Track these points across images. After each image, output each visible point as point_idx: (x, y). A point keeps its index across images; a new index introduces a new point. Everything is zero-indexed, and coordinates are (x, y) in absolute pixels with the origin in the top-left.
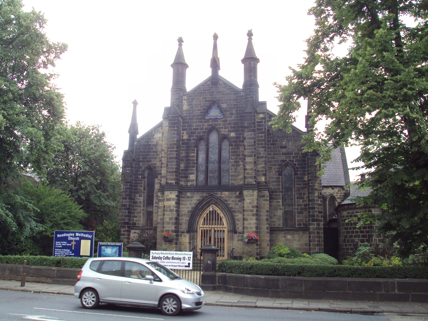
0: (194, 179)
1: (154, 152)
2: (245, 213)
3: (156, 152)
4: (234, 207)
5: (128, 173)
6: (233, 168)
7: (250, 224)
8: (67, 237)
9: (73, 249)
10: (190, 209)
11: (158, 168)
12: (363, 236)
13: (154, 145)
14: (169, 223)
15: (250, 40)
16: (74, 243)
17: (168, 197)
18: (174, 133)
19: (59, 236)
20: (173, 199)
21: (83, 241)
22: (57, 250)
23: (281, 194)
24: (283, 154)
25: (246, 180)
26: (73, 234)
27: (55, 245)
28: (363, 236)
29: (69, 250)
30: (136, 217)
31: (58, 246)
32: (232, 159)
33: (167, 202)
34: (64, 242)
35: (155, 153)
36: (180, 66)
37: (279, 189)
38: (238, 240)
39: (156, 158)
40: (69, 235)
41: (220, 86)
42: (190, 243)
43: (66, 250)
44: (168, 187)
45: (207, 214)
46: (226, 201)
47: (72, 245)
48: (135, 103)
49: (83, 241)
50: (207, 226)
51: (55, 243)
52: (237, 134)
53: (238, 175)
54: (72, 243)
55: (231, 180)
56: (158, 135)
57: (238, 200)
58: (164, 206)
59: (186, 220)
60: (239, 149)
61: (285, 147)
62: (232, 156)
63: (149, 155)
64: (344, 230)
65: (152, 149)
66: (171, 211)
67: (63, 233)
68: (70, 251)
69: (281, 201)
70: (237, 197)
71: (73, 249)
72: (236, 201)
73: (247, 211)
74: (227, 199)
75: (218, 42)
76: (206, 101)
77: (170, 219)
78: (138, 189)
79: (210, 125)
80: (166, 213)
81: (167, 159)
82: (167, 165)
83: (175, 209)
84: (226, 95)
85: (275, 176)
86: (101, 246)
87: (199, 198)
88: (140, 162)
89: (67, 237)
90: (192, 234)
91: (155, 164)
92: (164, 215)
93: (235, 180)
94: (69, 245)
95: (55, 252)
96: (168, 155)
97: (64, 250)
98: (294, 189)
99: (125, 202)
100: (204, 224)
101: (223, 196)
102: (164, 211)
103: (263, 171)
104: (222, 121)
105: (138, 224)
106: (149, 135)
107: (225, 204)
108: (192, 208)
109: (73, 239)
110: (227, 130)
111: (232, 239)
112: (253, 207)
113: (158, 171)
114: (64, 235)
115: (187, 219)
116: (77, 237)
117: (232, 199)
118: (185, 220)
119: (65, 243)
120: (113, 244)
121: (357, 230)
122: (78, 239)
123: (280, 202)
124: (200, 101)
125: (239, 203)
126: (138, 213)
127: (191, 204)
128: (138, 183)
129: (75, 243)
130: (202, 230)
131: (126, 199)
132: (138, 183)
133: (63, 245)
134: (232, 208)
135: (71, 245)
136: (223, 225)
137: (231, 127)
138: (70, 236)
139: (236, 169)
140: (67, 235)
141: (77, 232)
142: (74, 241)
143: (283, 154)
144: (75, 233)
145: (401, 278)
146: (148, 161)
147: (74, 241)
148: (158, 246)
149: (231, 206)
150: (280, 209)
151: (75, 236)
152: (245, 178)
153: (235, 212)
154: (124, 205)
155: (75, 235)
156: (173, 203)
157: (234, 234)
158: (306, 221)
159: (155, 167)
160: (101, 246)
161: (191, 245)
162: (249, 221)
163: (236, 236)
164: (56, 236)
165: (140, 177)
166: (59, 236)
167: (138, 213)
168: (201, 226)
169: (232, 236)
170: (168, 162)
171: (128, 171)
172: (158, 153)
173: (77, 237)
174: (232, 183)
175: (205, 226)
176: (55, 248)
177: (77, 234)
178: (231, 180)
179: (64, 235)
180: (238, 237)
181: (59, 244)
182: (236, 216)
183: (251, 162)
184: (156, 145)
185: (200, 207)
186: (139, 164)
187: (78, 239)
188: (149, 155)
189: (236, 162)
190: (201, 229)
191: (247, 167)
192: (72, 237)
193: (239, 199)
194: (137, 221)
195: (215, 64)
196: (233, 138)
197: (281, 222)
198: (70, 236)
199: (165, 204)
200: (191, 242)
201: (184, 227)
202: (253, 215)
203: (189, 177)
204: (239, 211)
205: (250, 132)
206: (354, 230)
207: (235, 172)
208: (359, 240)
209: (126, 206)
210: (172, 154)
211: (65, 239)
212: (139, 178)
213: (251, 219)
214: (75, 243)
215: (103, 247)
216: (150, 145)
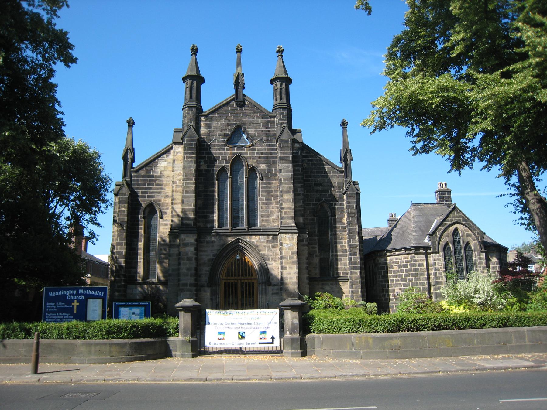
2: (284, 261)
3: (161, 185)
4: (266, 254)
6: (264, 206)
7: (290, 274)
8: (66, 295)
9: (75, 312)
10: (211, 257)
12: (404, 285)
13: (156, 177)
14: (187, 275)
16: (76, 304)
17: (184, 242)
18: (192, 161)
19: (51, 294)
20: (192, 244)
21: (90, 301)
23: (317, 238)
24: (318, 192)
25: (284, 221)
26: (75, 292)
27: (46, 308)
28: (404, 285)
31: (50, 310)
32: (262, 195)
33: (183, 249)
34: (60, 304)
37: (315, 232)
38: (273, 294)
39: (160, 193)
42: (212, 299)
43: (63, 314)
44: (184, 229)
45: (232, 263)
46: (257, 246)
47: (73, 306)
49: (90, 301)
50: (232, 278)
51: (46, 305)
52: (268, 166)
53: (270, 216)
54: (73, 304)
55: (262, 221)
56: (163, 163)
57: (271, 245)
58: (179, 253)
59: (206, 271)
60: (271, 184)
61: (320, 184)
62: (262, 191)
64: (381, 279)
65: (155, 181)
66: (189, 259)
67: (58, 290)
68: (71, 315)
69: (317, 246)
70: (269, 241)
71: (75, 312)
72: (269, 247)
73: (286, 258)
74: (258, 244)
76: (228, 124)
77: (188, 269)
79: (233, 154)
80: (182, 262)
81: (183, 193)
82: (183, 201)
83: (194, 257)
84: (254, 118)
85: (309, 218)
89: (66, 295)
90: (214, 288)
91: (160, 200)
92: (179, 264)
93: (267, 221)
94: (68, 306)
96: (183, 188)
97: (60, 314)
98: (330, 233)
99: (120, 249)
100: (229, 276)
101: (252, 240)
102: (179, 259)
103: (300, 210)
104: (249, 150)
107: (255, 250)
108: (214, 255)
109: (75, 298)
110: (256, 160)
111: (266, 293)
112: (292, 253)
113: (163, 209)
114: (60, 293)
115: (208, 269)
116: (81, 295)
117: (263, 244)
118: (205, 270)
119: (61, 305)
121: (397, 278)
122: (83, 297)
123: (315, 248)
124: (221, 124)
125: (273, 249)
127: (212, 251)
129: (78, 304)
130: (225, 283)
133: (58, 307)
134: (264, 255)
135: (71, 306)
136: (252, 275)
137: (261, 158)
138: (70, 295)
139: (268, 208)
140: (65, 292)
141: (81, 289)
142: (76, 301)
143: (318, 192)
144: (77, 290)
145: (131, 338)
146: (149, 197)
147: (76, 301)
148: (261, 299)
149: (263, 252)
150: (316, 256)
151: (78, 294)
152: (282, 218)
153: (269, 260)
154: (119, 252)
156: (191, 249)
157: (267, 287)
158: (346, 270)
159: (159, 205)
160: (118, 307)
161: (214, 301)
162: (289, 270)
163: (270, 288)
164: (47, 294)
166: (51, 294)
168: (224, 277)
169: (265, 289)
170: (183, 197)
171: (123, 209)
172: (163, 186)
173: (81, 295)
174: (264, 225)
175: (229, 278)
176: (46, 312)
177: (81, 291)
178: (262, 221)
179: (60, 293)
180: (273, 290)
181: (53, 307)
183: (288, 200)
185: (224, 255)
187: (83, 297)
188: (150, 189)
189: (267, 199)
190: (224, 281)
191: (285, 205)
192: (73, 295)
193: (272, 244)
195: (238, 83)
196: (264, 170)
197: (318, 271)
198: (70, 295)
199: (180, 250)
200: (214, 298)
201: (205, 279)
202: (293, 263)
203: (209, 217)
205: (287, 163)
206: (394, 279)
207: (267, 211)
208: (400, 289)
209: (122, 253)
210: (188, 187)
213: (291, 268)
214: (78, 304)
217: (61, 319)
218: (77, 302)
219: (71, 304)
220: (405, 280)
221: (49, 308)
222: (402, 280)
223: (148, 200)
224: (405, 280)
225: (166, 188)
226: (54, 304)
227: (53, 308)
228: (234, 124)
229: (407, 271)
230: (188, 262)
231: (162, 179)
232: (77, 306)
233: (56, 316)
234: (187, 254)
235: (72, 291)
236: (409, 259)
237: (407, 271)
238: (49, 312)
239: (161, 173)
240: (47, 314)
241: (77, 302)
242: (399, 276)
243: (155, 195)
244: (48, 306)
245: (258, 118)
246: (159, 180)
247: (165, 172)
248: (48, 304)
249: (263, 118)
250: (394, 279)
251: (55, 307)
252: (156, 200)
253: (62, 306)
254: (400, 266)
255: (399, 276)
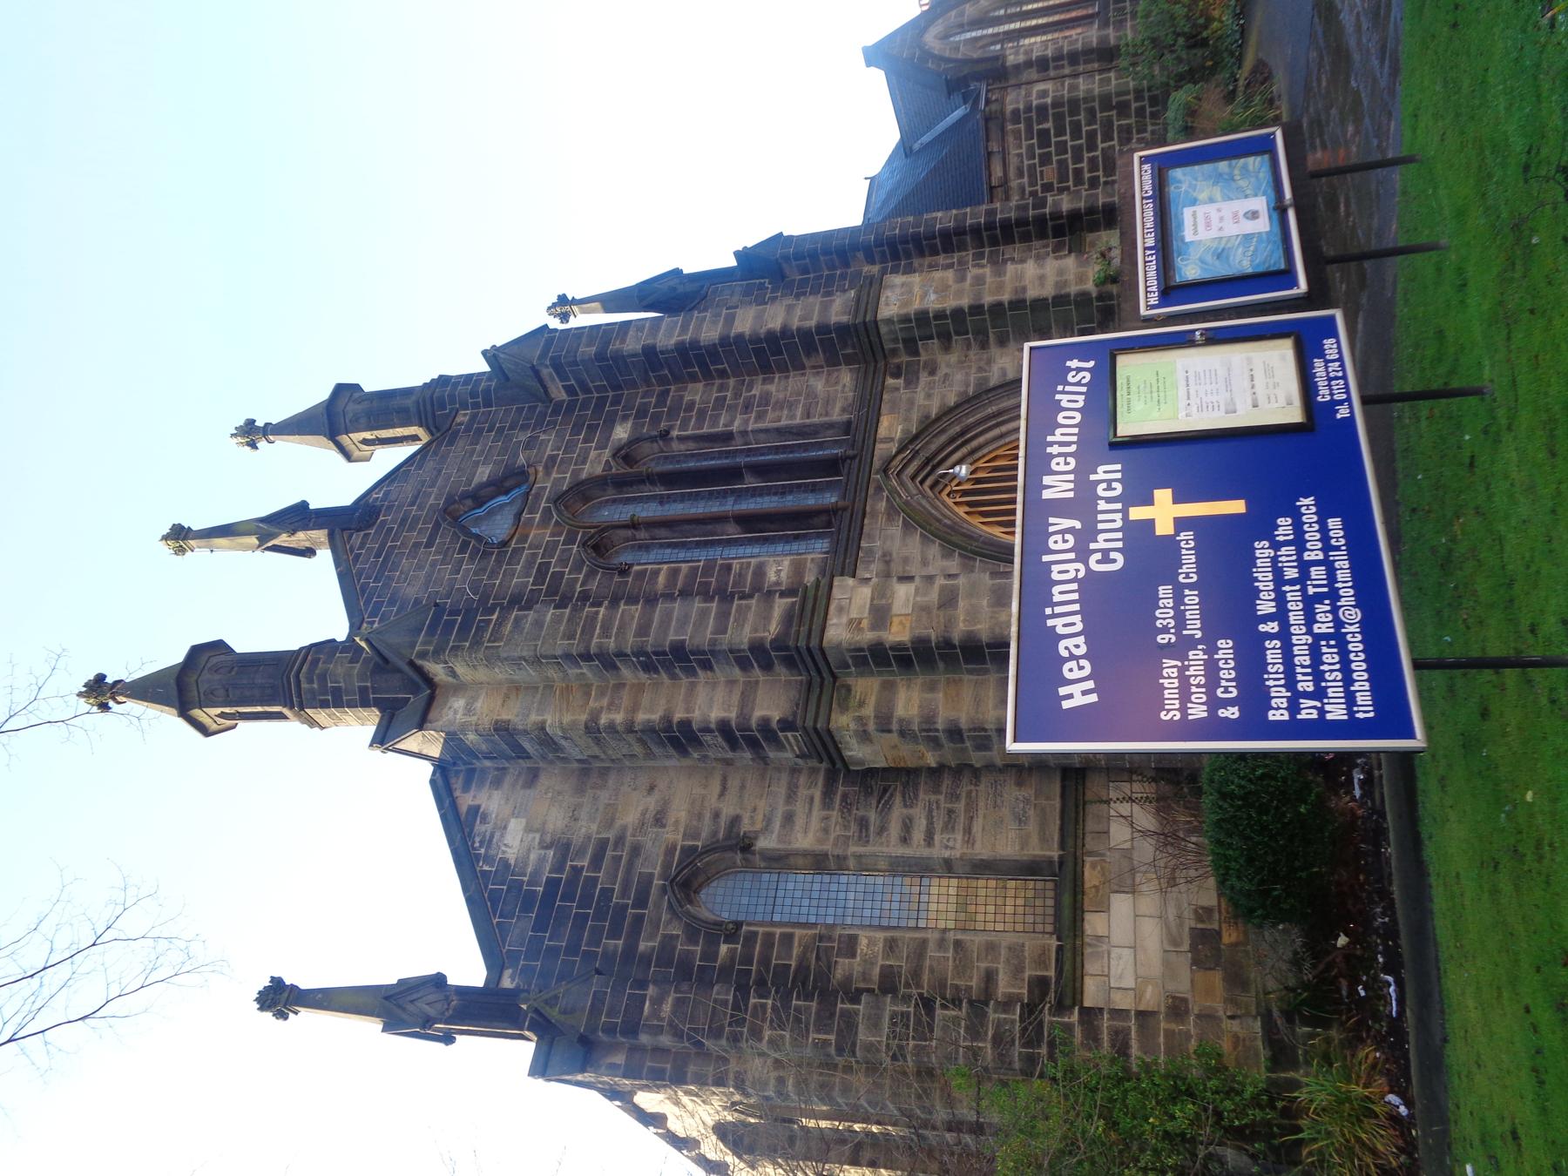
0: (792, 563)
1: (596, 862)
5: (679, 1003)
8: (1090, 586)
9: (1237, 507)
11: (696, 836)
15: (270, 431)
16: (1164, 511)
17: (865, 624)
19: (1077, 694)
22: (1279, 697)
29: (1262, 550)
30: (990, 977)
34: (1164, 615)
35: (609, 853)
36: (212, 685)
39: (636, 850)
40: (1065, 571)
41: (393, 497)
47: (1181, 524)
48: (279, 998)
54: (1164, 528)
56: (508, 839)
63: (607, 893)
65: (577, 871)
67: (1042, 643)
68: (1268, 533)
71: (1237, 507)
75: (197, 525)
78: (803, 968)
86: (1169, 291)
87: (896, 530)
88: (631, 949)
91: (670, 851)
95: (1323, 728)
97: (1266, 606)
99: (875, 1025)
105: (1041, 961)
106: (489, 893)
109: (1110, 519)
113: (715, 833)
120: (1144, 218)
121: (1084, 165)
126: (963, 966)
128: (765, 961)
129: (1163, 496)
131: (849, 1021)
132: (765, 961)
133: (1194, 628)
138: (1082, 554)
141: (1034, 486)
142: (1137, 513)
146: (641, 901)
147: (1137, 513)
151: (1083, 504)
155: (1060, 508)
165: (724, 948)
167: (963, 966)
171: (667, 1008)
174: (844, 410)
177: (1058, 487)
181: (1196, 672)
182: (1005, 374)
184: (563, 848)
186: (646, 960)
188: (607, 893)
192: (1085, 536)
194: (1018, 970)
198: (1082, 554)
204: (980, 369)
211: (1119, 608)
212: (732, 952)
214: (1163, 496)
215: (1189, 271)
216: (552, 884)
217: (1309, 603)
218: (1149, 501)
219: (1171, 543)
220: (1092, 136)
221: (1214, 704)
222: (1092, 146)
223: (658, 906)
224: (1092, 136)
225: (618, 823)
226: (1170, 667)
227: (1212, 668)
228: (437, 526)
229: (1060, 131)
230: (962, 604)
231: (577, 840)
232: (1177, 500)
233: (1284, 635)
234: (924, 609)
235: (1055, 542)
236: (1022, 126)
237: (1060, 131)
238: (1254, 695)
239: (547, 848)
240: (1278, 715)
241: (1149, 501)
242: (1078, 158)
243: (641, 868)
244: (1198, 711)
245: (444, 458)
246: (581, 852)
247: (550, 827)
248: (1170, 714)
249: (451, 443)
250: (1087, 175)
251: (1197, 655)
252: (667, 866)
253: (1192, 598)
254: (1045, 160)
255: (1078, 158)
